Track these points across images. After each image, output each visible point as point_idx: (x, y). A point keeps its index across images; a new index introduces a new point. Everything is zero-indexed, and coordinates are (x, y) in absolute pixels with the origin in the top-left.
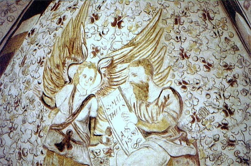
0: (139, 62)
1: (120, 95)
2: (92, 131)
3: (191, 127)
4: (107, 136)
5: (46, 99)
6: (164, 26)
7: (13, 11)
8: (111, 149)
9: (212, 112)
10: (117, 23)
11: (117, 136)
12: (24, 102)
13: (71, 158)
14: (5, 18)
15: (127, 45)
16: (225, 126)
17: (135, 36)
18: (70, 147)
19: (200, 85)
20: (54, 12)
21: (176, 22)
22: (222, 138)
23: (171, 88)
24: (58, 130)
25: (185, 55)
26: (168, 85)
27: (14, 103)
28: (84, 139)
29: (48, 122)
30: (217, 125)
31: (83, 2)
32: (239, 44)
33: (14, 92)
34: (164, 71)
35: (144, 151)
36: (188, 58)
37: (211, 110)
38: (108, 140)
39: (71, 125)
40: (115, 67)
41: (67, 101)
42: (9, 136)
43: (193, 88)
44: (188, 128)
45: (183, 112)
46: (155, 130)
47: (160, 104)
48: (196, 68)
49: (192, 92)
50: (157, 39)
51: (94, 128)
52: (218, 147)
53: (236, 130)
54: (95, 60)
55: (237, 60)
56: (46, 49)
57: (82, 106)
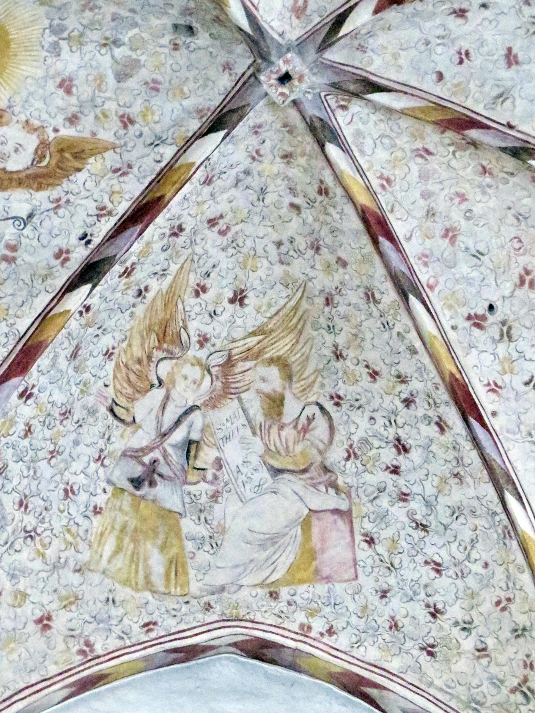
0: (272, 361)
1: (240, 410)
2: (191, 462)
3: (344, 466)
4: (214, 471)
5: (117, 409)
6: (309, 307)
7: (56, 277)
8: (218, 492)
9: (377, 446)
10: (239, 298)
11: (229, 472)
12: (78, 414)
13: (154, 501)
14: (42, 287)
15: (254, 334)
16: (395, 470)
17: (266, 320)
18: (152, 484)
19: (361, 402)
20: (124, 280)
21: (328, 302)
22: (390, 488)
23: (318, 404)
24: (135, 457)
25: (341, 353)
26: (313, 399)
27: (60, 414)
28: (178, 473)
29: (118, 445)
30: (384, 467)
31: (178, 267)
32: (418, 344)
33: (59, 397)
34: (308, 377)
35: (269, 498)
36: (345, 359)
37: (376, 443)
38: (216, 477)
39: (157, 451)
40: (233, 366)
41: (154, 413)
42: (49, 464)
43: (351, 406)
44: (339, 468)
45: (334, 442)
46: (290, 467)
47: (300, 427)
48: (355, 376)
49: (349, 413)
50: (299, 327)
51: (195, 457)
52: (384, 502)
53: (412, 477)
54: (202, 354)
55: (415, 368)
56: (116, 334)
57: (178, 422)
